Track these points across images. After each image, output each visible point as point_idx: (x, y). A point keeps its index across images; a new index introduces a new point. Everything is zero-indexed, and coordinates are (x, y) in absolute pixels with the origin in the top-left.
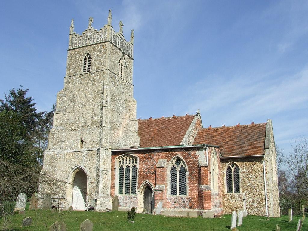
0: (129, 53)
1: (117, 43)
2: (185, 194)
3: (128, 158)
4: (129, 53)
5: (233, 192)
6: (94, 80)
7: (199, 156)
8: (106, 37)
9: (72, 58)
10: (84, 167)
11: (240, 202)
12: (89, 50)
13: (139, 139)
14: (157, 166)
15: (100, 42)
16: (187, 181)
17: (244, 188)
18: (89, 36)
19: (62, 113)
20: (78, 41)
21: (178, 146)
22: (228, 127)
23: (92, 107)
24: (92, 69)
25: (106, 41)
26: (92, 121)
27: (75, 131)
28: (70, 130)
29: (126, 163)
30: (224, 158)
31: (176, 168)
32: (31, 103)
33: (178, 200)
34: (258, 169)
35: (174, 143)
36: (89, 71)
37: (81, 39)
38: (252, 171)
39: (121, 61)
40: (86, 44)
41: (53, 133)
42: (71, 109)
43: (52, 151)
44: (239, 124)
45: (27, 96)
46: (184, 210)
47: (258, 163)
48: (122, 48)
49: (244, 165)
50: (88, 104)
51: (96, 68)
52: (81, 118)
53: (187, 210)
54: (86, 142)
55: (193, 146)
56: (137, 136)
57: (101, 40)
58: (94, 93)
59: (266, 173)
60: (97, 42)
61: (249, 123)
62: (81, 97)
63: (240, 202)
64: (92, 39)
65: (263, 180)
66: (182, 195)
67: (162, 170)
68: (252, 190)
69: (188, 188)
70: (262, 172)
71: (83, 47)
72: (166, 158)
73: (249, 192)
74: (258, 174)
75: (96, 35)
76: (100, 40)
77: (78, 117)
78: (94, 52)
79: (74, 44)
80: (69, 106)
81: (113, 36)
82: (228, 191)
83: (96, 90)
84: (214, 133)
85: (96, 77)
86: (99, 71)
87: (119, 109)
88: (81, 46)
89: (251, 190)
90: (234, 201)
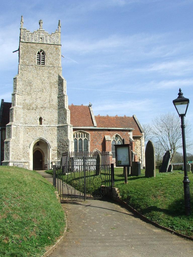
3: (80, 133)
6: (50, 73)
9: (24, 50)
12: (44, 48)
19: (20, 94)
22: (111, 117)
23: (49, 93)
24: (47, 64)
26: (50, 104)
27: (34, 111)
28: (28, 110)
40: (39, 42)
41: (16, 110)
43: (16, 124)
44: (117, 115)
47: (138, 140)
50: (44, 91)
52: (39, 101)
54: (45, 120)
59: (142, 146)
61: (123, 116)
62: (37, 83)
64: (45, 39)
65: (140, 150)
70: (140, 145)
71: (36, 43)
75: (48, 37)
77: (36, 99)
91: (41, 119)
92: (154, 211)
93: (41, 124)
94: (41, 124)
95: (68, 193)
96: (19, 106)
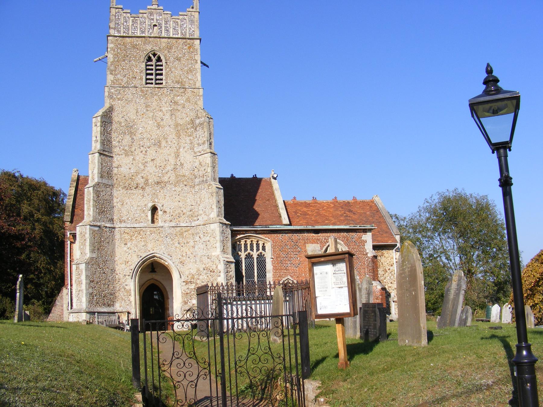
6: (176, 103)
7: (366, 241)
10: (169, 255)
15: (179, 36)
18: (155, 20)
19: (107, 153)
20: (131, 24)
21: (325, 226)
29: (258, 250)
31: (257, 258)
34: (386, 261)
42: (126, 148)
50: (163, 143)
51: (178, 82)
52: (151, 168)
54: (165, 212)
55: (359, 227)
58: (177, 125)
64: (163, 28)
72: (318, 243)
76: (179, 32)
77: (145, 164)
83: (181, 122)
84: (305, 209)
85: (178, 98)
86: (184, 88)
88: (139, 35)
96: (107, 181)
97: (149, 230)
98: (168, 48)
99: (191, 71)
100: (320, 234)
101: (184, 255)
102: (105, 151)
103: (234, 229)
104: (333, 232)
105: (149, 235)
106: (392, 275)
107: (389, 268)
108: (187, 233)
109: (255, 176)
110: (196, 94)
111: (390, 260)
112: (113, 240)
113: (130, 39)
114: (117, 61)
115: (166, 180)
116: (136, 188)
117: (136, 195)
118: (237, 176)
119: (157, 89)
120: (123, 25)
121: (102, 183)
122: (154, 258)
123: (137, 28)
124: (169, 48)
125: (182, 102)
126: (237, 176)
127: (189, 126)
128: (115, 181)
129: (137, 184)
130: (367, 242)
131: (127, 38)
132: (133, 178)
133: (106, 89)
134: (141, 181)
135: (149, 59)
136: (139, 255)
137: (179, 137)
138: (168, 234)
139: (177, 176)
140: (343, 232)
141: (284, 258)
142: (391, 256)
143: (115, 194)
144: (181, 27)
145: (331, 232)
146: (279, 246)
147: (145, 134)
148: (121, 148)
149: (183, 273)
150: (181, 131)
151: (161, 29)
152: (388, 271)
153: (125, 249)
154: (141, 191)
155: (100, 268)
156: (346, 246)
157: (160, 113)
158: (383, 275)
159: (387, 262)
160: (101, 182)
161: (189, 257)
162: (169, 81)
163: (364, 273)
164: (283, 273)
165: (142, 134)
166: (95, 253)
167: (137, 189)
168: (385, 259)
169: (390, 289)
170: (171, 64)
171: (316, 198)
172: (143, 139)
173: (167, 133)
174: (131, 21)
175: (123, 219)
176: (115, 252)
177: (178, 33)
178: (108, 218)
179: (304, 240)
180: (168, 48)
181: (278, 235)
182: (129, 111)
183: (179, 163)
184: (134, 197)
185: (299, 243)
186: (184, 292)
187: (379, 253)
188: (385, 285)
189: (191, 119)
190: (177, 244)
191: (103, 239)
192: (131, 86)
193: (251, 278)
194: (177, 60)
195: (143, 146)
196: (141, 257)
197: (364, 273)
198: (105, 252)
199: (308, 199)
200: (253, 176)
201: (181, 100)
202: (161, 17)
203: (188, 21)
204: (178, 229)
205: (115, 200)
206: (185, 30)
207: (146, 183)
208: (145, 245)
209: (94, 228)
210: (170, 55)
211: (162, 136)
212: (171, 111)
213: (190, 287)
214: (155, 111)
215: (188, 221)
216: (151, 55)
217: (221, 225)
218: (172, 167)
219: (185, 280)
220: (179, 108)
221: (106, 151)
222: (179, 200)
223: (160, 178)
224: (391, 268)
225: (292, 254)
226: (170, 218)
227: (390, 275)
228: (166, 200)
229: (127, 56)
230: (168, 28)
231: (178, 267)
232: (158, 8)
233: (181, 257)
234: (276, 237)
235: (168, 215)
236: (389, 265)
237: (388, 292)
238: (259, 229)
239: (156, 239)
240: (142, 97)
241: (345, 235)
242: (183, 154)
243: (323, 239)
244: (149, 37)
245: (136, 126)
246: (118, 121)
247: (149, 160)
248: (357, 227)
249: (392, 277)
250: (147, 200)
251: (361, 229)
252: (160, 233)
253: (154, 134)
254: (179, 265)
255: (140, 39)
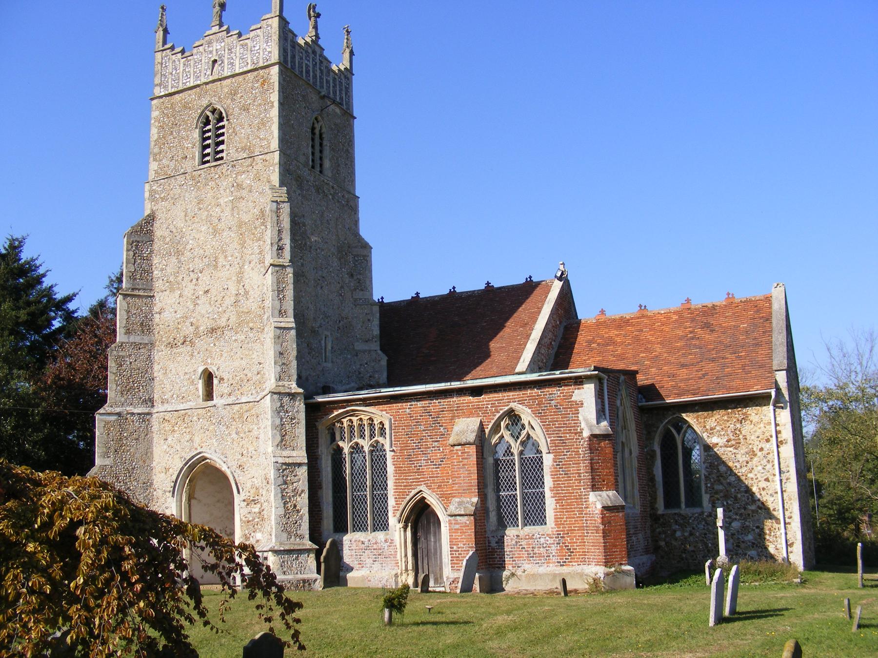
0: (341, 98)
1: (302, 67)
2: (542, 521)
4: (341, 98)
5: (683, 506)
6: (240, 186)
7: (582, 404)
8: (269, 52)
11: (705, 534)
13: (384, 362)
14: (451, 441)
15: (249, 68)
16: (548, 481)
17: (716, 493)
18: (214, 53)
19: (141, 293)
21: (475, 381)
24: (229, 150)
25: (269, 62)
29: (372, 436)
30: (651, 405)
32: (41, 271)
33: (524, 543)
34: (755, 432)
35: (495, 370)
36: (222, 158)
37: (192, 63)
38: (739, 439)
39: (318, 127)
41: (119, 357)
45: (25, 255)
46: (542, 570)
48: (318, 83)
49: (713, 425)
50: (221, 261)
51: (244, 149)
52: (204, 307)
53: (552, 568)
55: (561, 373)
56: (380, 352)
57: (252, 60)
58: (241, 224)
60: (241, 71)
63: (705, 534)
64: (226, 62)
66: (534, 525)
67: (468, 452)
68: (739, 496)
69: (550, 504)
71: (198, 86)
73: (729, 502)
74: (755, 449)
75: (238, 48)
76: (249, 61)
78: (233, 100)
79: (170, 80)
80: (162, 270)
81: (289, 48)
82: (667, 505)
83: (246, 218)
84: (614, 333)
86: (251, 157)
87: (320, 273)
88: (192, 85)
89: (736, 498)
90: (686, 534)
91: (208, 378)
92: (690, 458)
93: (209, 395)
94: (209, 395)
95: (470, 515)
96: (139, 337)
97: (196, 412)
98: (232, 94)
99: (264, 124)
100: (483, 396)
101: (244, 453)
102: (137, 289)
103: (320, 400)
104: (510, 390)
105: (196, 421)
106: (768, 461)
107: (760, 447)
108: (248, 414)
109: (452, 290)
110: (269, 163)
111: (763, 429)
112: (147, 435)
113: (181, 95)
114: (163, 137)
115: (223, 324)
116: (183, 344)
117: (183, 355)
118: (426, 293)
119: (212, 169)
120: (171, 76)
121: (127, 343)
122: (207, 461)
123: (190, 75)
124: (233, 93)
125: (249, 182)
126: (496, 284)
127: (258, 223)
128: (156, 335)
129: (185, 337)
130: (585, 405)
131: (176, 96)
132: (180, 326)
133: (147, 187)
134: (188, 330)
135: (207, 122)
136: (182, 457)
137: (243, 245)
138: (221, 418)
139: (239, 314)
140: (530, 388)
141: (413, 449)
142: (765, 420)
143: (156, 357)
144: (251, 51)
145: (505, 391)
146: (405, 426)
147: (196, 250)
148: (165, 279)
149: (242, 485)
150: (246, 233)
151: (223, 65)
152: (759, 454)
153: (165, 447)
154: (189, 348)
155: (120, 482)
156: (536, 416)
157: (217, 210)
158: (747, 462)
159: (757, 434)
160: (127, 341)
161: (251, 457)
162: (231, 152)
163: (576, 473)
164: (413, 479)
165: (192, 251)
166: (108, 457)
167: (185, 345)
168: (753, 426)
169: (762, 492)
170: (235, 120)
171: (645, 307)
172: (194, 258)
173: (227, 241)
174: (182, 65)
175: (166, 397)
176: (152, 453)
177: (247, 63)
178: (141, 398)
179: (452, 411)
180: (232, 94)
181: (404, 404)
182: (176, 215)
183: (242, 291)
184: (180, 358)
185: (443, 417)
186: (244, 519)
187: (737, 416)
188: (752, 486)
189: (262, 209)
190: (234, 436)
191: (125, 434)
192: (181, 173)
193: (362, 490)
194: (244, 110)
195: (193, 271)
196: (185, 459)
197: (576, 473)
198: (129, 455)
199: (629, 310)
200: (527, 279)
201: (246, 180)
202: (223, 44)
203: (262, 37)
204: (236, 407)
205: (156, 367)
206: (257, 55)
207: (197, 334)
208: (191, 440)
209: (107, 417)
210: (234, 104)
211: (220, 248)
212: (232, 201)
213: (254, 510)
214: (210, 207)
215: (254, 392)
216: (209, 114)
217: (275, 396)
218: (233, 299)
219: (246, 497)
220: (244, 193)
221: (139, 290)
222: (241, 356)
223: (216, 321)
224: (766, 446)
225: (428, 442)
226: (228, 389)
227: (764, 462)
228: (223, 359)
229: (176, 125)
230: (232, 59)
231: (235, 474)
232: (220, 30)
233: (240, 457)
234: (400, 409)
235: (226, 385)
236: (762, 439)
237: (759, 500)
238: (361, 396)
239: (205, 428)
240: (192, 188)
241: (535, 393)
242: (248, 274)
243: (489, 406)
244: (204, 83)
245: (184, 239)
246: (161, 236)
247: (201, 293)
248: (554, 374)
249: (769, 466)
250: (197, 362)
251: (570, 378)
252: (210, 417)
253: (209, 247)
254: (237, 471)
255: (194, 90)
